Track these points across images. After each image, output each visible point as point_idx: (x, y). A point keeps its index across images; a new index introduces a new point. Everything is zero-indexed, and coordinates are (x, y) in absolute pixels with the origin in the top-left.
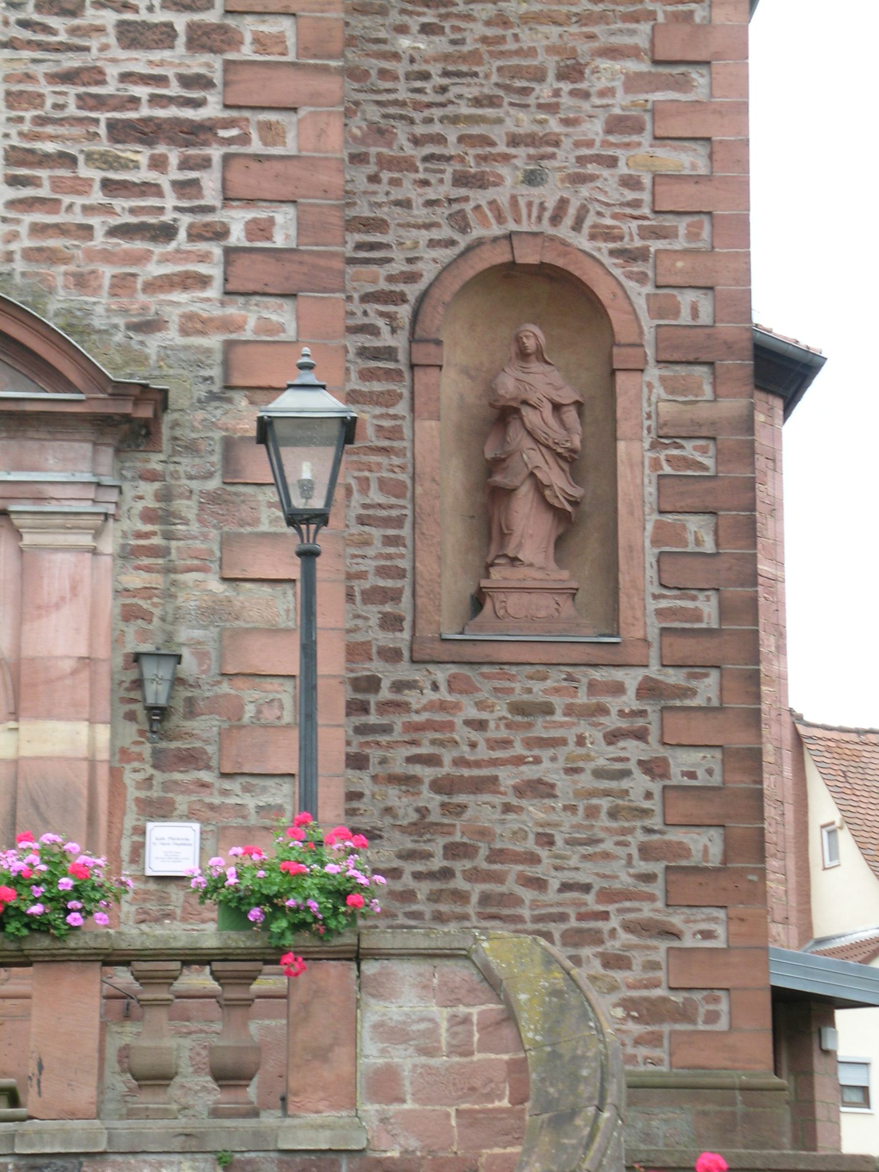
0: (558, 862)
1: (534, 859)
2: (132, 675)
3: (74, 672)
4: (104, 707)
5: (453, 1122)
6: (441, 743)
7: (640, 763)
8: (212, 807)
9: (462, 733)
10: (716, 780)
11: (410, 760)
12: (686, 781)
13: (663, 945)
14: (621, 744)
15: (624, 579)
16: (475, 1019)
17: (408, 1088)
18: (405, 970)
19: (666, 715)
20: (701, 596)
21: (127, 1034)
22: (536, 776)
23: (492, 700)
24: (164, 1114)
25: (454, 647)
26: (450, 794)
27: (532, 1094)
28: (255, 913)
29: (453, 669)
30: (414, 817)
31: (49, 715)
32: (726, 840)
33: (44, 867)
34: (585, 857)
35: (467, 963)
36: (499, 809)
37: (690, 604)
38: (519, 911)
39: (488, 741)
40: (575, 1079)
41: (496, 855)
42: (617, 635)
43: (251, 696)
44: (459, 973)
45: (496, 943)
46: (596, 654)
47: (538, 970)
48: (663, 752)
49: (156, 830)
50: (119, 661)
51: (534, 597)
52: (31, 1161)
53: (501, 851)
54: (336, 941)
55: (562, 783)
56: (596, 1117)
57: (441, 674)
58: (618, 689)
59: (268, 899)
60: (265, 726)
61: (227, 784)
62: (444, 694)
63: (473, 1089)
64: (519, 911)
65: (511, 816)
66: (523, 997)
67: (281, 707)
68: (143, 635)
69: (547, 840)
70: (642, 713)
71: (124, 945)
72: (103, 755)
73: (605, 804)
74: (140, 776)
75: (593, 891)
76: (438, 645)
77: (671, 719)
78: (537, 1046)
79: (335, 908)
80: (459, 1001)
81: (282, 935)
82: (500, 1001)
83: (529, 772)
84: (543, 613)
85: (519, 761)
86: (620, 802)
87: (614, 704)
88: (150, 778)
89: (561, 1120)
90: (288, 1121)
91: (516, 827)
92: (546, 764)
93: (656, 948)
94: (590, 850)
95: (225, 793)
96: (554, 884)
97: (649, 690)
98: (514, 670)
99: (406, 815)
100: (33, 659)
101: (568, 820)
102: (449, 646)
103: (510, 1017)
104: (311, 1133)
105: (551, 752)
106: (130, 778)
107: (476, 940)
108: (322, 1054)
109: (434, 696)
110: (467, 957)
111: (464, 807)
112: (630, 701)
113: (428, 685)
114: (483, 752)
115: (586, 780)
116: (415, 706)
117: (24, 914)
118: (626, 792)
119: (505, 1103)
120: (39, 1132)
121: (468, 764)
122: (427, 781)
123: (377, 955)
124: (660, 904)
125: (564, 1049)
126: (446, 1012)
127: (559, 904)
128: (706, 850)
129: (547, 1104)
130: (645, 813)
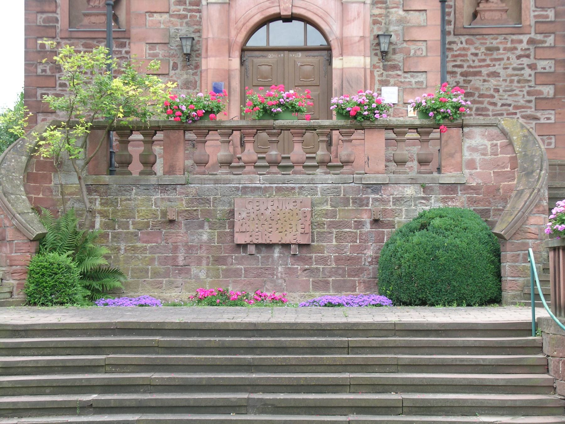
0: (501, 97)
1: (493, 96)
2: (376, 41)
3: (359, 41)
4: (368, 52)
5: (492, 175)
6: (463, 61)
7: (527, 65)
8: (401, 82)
9: (470, 57)
10: (552, 70)
11: (454, 66)
12: (542, 71)
13: (534, 122)
14: (521, 59)
15: (523, 6)
16: (499, 145)
17: (478, 165)
18: (477, 130)
19: (537, 49)
20: (549, 10)
21: (391, 152)
22: (494, 70)
23: (480, 47)
24: (405, 173)
25: (468, 30)
26: (466, 77)
27: (519, 166)
28: (431, 114)
29: (467, 37)
30: (455, 84)
31: (352, 54)
32: (555, 89)
33: (368, 101)
34: (509, 96)
35: (496, 128)
36: (482, 81)
37: (545, 13)
38: (488, 113)
39: (478, 60)
40: (532, 162)
41: (481, 96)
42: (521, 24)
43: (413, 47)
44: (494, 131)
45: (506, 122)
46: (514, 31)
47: (519, 129)
48: (535, 61)
49: (384, 89)
50: (372, 37)
51: (494, 13)
52: (367, 186)
53: (483, 94)
54: (455, 122)
55: (502, 72)
56: (540, 173)
57: (463, 39)
58: (521, 42)
59: (435, 110)
60: (418, 57)
61: (406, 75)
62: (464, 45)
63: (498, 165)
64: (488, 113)
65: (486, 83)
66: (515, 138)
67: (422, 50)
68: (379, 29)
69: (497, 91)
70: (528, 49)
71: (391, 124)
72: (368, 67)
73: (516, 78)
74: (379, 73)
75: (512, 106)
76: (462, 29)
77: (538, 51)
78: (520, 152)
79: (456, 112)
80: (494, 139)
81: (439, 120)
82: (507, 139)
83: (491, 69)
84: (496, 18)
85: (488, 66)
86: (521, 78)
87: (519, 46)
88: (382, 73)
89: (529, 174)
90: (442, 175)
91: (487, 86)
92: (497, 66)
93: (532, 123)
94: (511, 93)
95: (405, 78)
96: (499, 104)
97: (531, 41)
98: (487, 37)
99: (452, 84)
100: (347, 37)
101: (504, 84)
102: (466, 30)
103: (511, 143)
104: (449, 178)
105: (499, 63)
106: (376, 74)
107: (499, 121)
108: (452, 155)
109: (461, 46)
110: (496, 126)
111: (471, 81)
112: (524, 45)
113: (459, 42)
114: (477, 63)
115: (510, 71)
116: (455, 49)
117: (362, 114)
118: (523, 75)
119: (509, 169)
120: (369, 178)
121: (472, 67)
122: (459, 73)
123: (468, 126)
124: (533, 110)
125: (528, 153)
126: (490, 143)
127: (501, 110)
128: (548, 92)
129: (524, 169)
130: (529, 81)
